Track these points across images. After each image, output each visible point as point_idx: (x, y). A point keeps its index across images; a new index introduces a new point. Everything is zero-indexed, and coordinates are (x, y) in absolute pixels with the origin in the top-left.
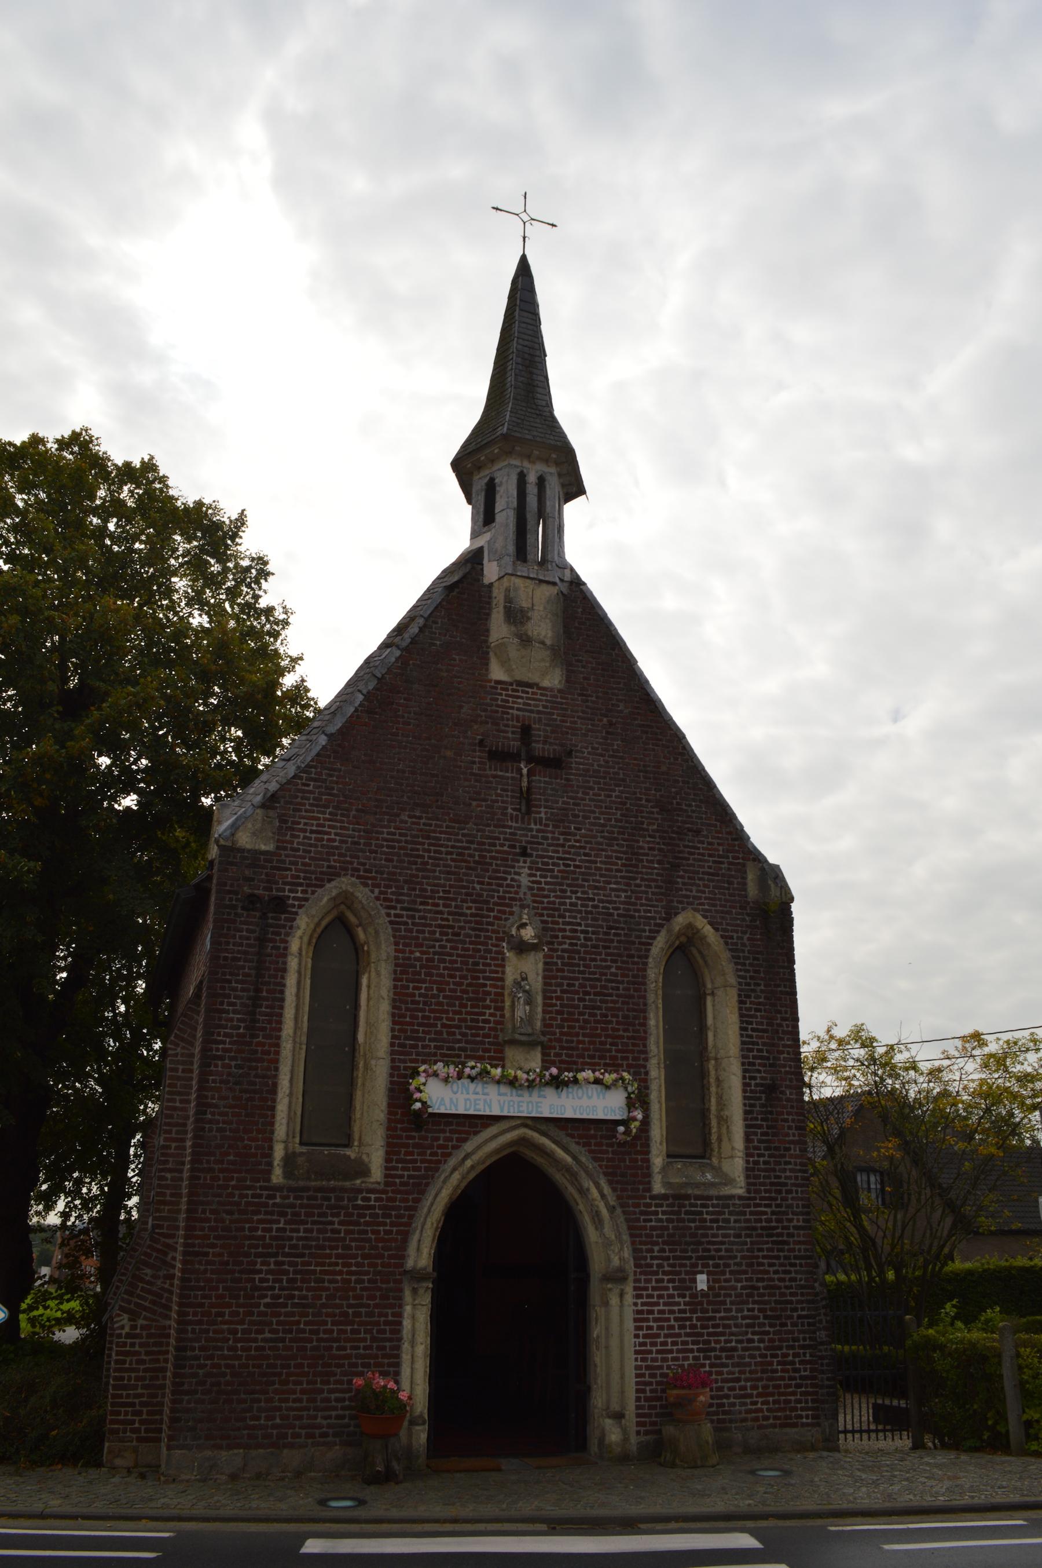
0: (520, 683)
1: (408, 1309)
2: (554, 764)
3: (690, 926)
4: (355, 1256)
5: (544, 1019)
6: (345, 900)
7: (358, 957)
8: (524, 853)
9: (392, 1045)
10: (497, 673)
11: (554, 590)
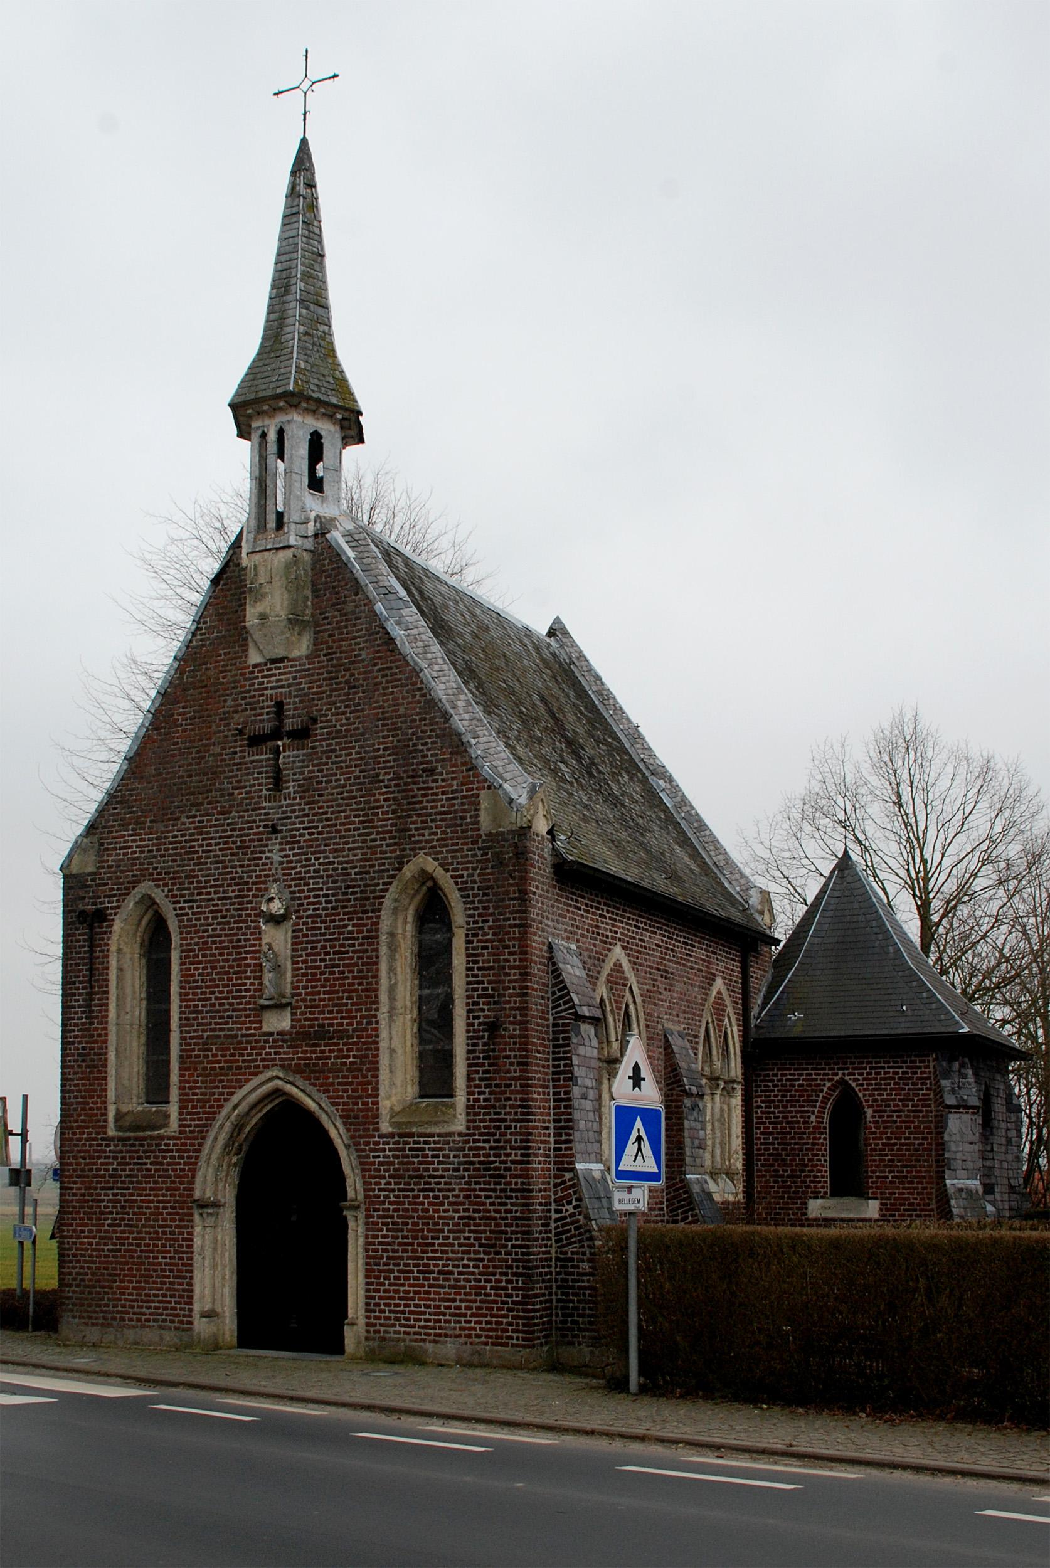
11: (288, 553)
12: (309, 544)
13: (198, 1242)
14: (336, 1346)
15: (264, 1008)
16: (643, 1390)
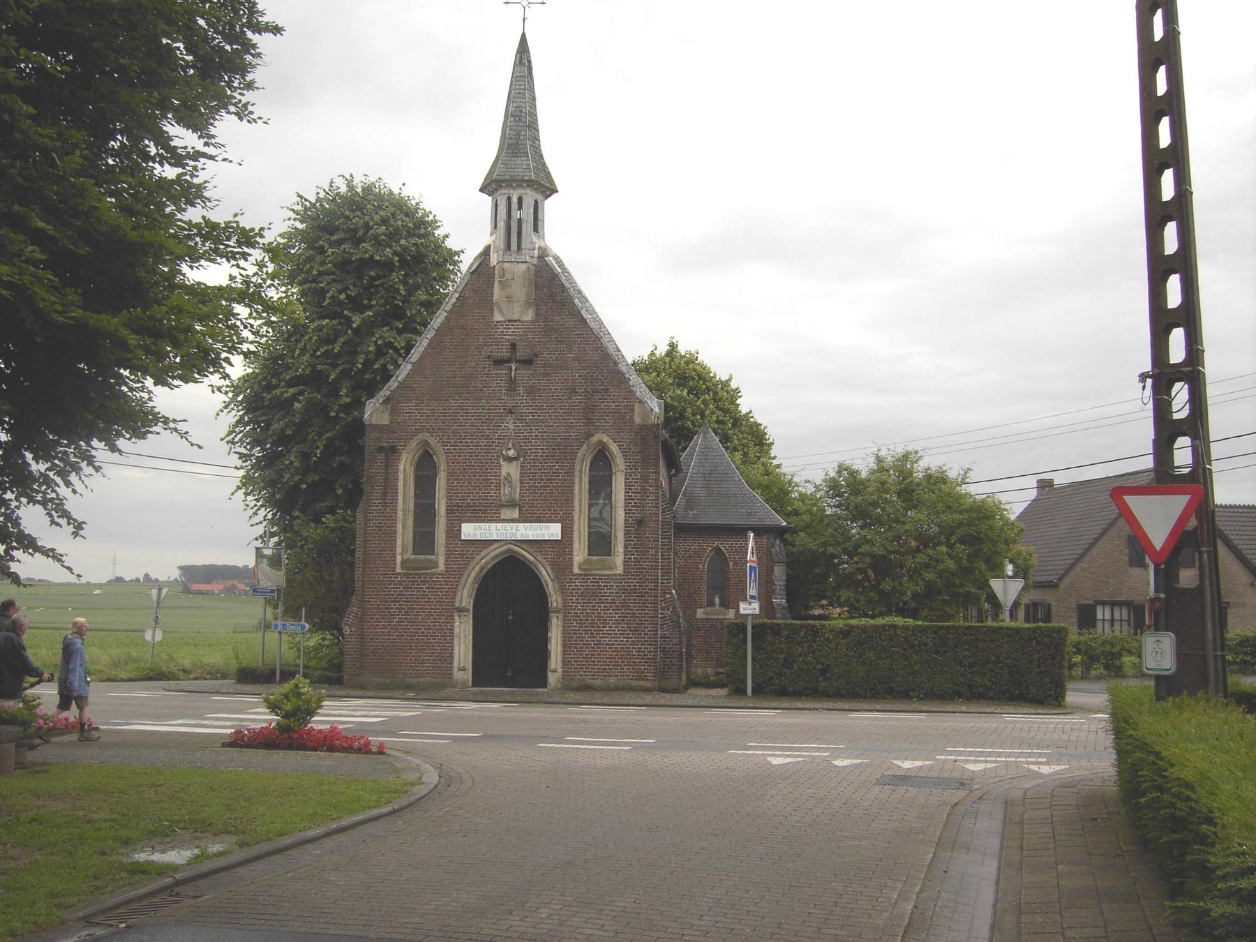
2: (527, 362)
3: (601, 442)
7: (434, 467)
8: (511, 412)
10: (498, 317)
11: (525, 266)
12: (535, 261)
13: (457, 630)
14: (543, 683)
15: (502, 506)
16: (758, 691)
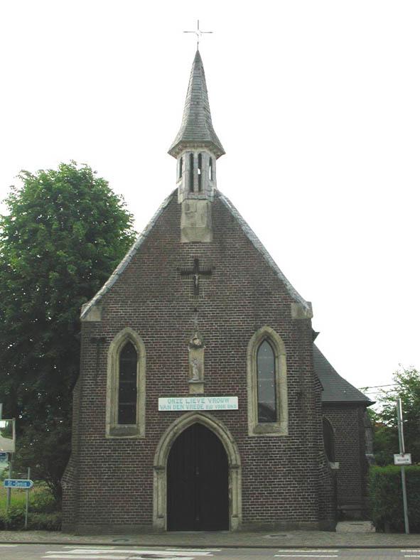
0: (193, 243)
1: (155, 479)
4: (135, 462)
5: (204, 374)
6: (129, 336)
8: (196, 311)
9: (146, 387)
10: (184, 240)
